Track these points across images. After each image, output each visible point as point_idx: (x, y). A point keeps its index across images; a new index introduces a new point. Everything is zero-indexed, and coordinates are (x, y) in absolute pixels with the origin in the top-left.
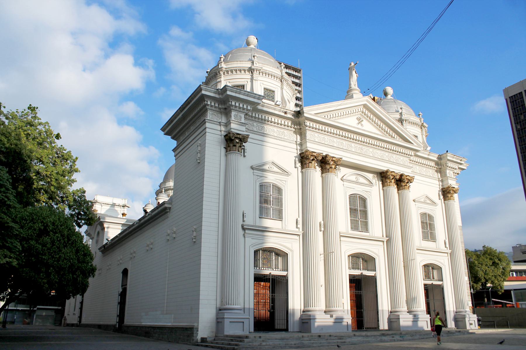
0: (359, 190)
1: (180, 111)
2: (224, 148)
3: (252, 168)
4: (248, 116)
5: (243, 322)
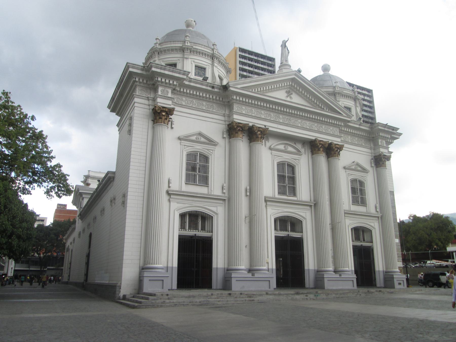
0: (287, 158)
1: (118, 89)
2: (152, 120)
3: (179, 139)
4: (176, 91)
5: (269, 281)
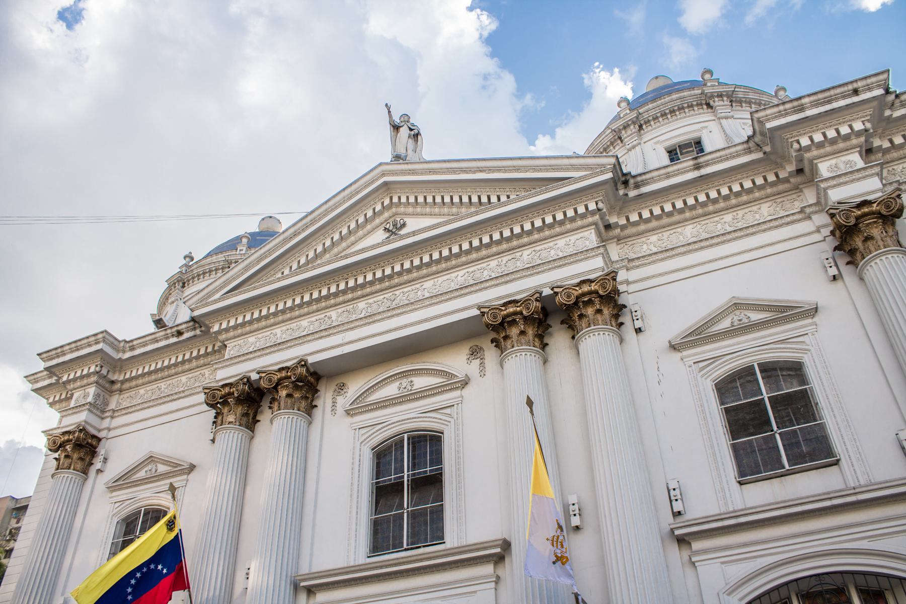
2: (848, 263)
4: (618, 231)
